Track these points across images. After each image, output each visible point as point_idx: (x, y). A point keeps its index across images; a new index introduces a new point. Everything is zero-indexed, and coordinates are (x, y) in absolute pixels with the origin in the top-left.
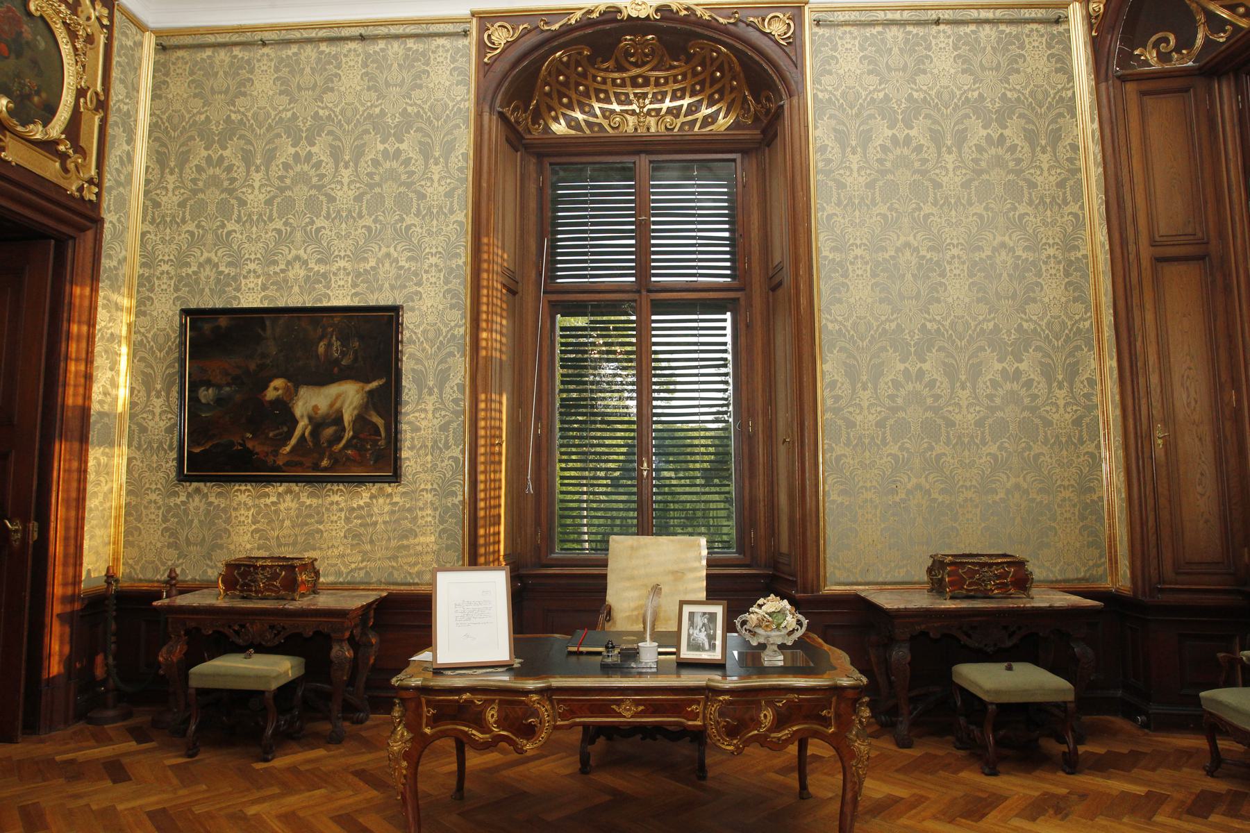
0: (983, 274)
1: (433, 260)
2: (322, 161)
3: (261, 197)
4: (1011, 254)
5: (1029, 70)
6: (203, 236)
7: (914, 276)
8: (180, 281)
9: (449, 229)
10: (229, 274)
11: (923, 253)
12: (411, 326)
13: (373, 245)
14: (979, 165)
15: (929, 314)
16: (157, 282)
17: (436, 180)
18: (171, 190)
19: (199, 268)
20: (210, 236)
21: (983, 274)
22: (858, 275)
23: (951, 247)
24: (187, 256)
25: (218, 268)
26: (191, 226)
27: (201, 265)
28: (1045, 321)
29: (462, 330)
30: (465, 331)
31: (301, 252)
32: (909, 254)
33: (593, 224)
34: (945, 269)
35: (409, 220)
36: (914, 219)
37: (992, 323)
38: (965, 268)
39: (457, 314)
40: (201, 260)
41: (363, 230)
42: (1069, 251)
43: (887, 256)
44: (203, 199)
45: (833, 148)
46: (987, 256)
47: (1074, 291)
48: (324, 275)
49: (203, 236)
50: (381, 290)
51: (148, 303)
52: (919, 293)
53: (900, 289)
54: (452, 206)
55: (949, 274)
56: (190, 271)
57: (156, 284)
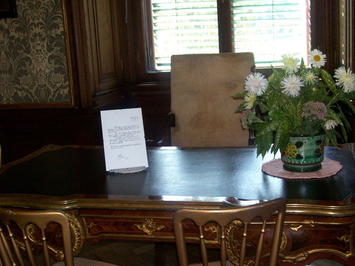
1: (37, 30)
7: (6, 53)
10: (19, 38)
15: (19, 85)
23: (33, 27)
25: (9, 33)
28: (34, 89)
29: (66, 91)
30: (70, 91)
39: (60, 77)
42: (50, 29)
47: (55, 64)
48: (24, 42)
55: (32, 50)
57: (32, 45)
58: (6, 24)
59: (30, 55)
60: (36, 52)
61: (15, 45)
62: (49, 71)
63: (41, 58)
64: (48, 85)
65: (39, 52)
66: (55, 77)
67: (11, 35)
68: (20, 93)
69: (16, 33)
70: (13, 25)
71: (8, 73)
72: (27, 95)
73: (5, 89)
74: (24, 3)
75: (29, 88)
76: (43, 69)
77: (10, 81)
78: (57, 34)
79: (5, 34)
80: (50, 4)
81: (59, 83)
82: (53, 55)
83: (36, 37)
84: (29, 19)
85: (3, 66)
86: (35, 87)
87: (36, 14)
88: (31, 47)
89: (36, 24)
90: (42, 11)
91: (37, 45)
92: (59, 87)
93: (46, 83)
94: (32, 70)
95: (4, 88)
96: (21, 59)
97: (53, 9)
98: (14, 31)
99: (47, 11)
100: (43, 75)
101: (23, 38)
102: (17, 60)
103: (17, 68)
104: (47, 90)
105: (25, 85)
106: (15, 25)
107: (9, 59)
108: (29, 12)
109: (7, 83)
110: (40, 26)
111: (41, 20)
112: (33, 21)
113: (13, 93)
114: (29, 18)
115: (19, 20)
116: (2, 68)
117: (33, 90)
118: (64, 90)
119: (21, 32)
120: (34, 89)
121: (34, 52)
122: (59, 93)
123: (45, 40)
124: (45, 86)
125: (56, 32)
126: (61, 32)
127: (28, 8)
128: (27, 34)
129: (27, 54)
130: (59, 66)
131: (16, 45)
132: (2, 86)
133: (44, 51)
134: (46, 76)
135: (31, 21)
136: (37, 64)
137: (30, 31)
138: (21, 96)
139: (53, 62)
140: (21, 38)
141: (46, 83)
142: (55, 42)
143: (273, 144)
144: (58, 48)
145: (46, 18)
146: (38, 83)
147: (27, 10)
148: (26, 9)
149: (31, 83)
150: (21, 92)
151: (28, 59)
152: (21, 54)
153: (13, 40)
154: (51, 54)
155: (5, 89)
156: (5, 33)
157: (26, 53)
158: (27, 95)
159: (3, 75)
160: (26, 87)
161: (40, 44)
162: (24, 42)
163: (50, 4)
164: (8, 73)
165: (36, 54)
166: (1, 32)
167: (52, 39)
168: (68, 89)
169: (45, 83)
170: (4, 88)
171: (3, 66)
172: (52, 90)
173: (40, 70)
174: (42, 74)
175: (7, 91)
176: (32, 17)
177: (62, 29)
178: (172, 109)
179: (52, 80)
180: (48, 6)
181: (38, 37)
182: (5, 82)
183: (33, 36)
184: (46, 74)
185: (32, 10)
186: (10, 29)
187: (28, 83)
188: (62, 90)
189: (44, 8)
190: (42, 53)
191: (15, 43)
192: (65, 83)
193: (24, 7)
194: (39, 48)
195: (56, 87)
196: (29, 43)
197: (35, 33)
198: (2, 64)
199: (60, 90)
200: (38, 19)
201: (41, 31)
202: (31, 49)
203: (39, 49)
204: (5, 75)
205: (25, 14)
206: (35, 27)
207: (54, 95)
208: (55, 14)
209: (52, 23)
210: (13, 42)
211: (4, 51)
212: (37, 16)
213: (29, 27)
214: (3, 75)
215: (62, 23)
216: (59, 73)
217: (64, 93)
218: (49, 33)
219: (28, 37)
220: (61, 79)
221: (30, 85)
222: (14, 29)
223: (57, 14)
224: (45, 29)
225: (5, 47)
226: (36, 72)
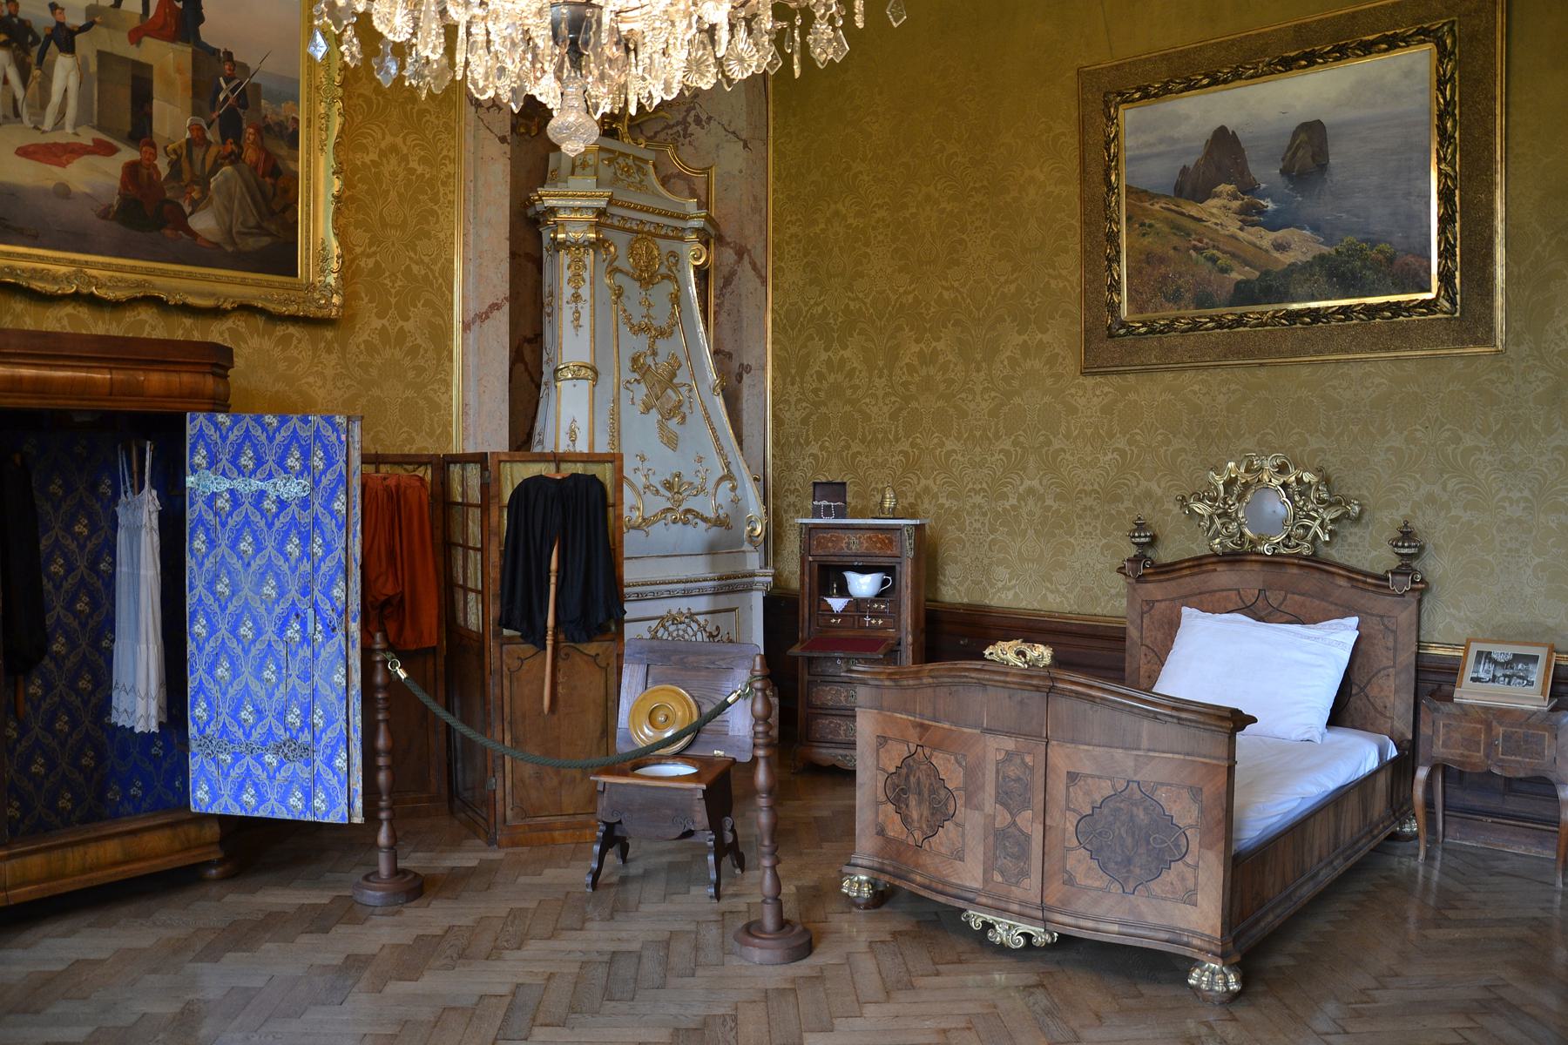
2: (855, 368)
4: (1039, 504)
5: (786, 286)
11: (1049, 502)
12: (954, 582)
14: (908, 390)
23: (1507, 504)
26: (1007, 444)
28: (965, 586)
38: (986, 522)
41: (1115, 455)
45: (956, 365)
50: (1024, 536)
53: (1020, 548)
56: (1122, 508)
57: (1077, 524)
64: (1096, 589)
72: (1062, 602)
84: (442, 149)
91: (1086, 524)
93: (1095, 586)
99: (995, 473)
106: (1464, 496)
108: (872, 472)
110: (1093, 496)
120: (965, 586)
125: (1117, 507)
135: (873, 485)
141: (1095, 586)
143: (881, 656)
154: (1542, 560)
172: (805, 309)
180: (1547, 467)
194: (978, 525)
201: (983, 501)
206: (1511, 505)
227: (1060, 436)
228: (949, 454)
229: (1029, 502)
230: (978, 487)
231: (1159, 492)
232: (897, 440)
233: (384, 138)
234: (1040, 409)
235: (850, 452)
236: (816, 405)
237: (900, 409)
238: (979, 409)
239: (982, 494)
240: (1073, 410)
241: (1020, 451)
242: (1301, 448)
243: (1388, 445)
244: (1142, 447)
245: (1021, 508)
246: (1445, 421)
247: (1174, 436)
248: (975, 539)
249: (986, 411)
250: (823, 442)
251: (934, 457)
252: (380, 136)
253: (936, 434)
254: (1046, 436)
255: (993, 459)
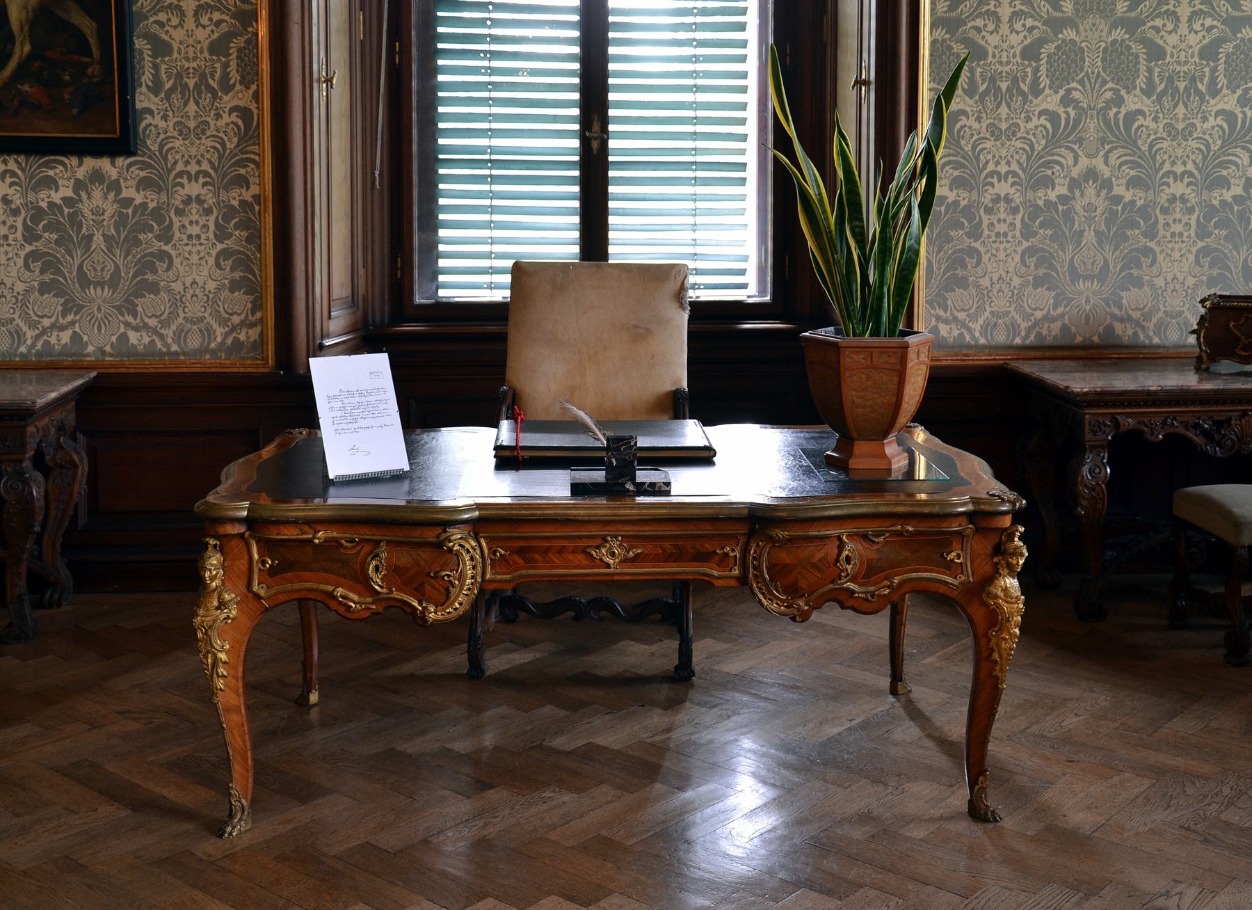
0: (54, 236)
1: (194, 189)
3: (1015, 39)
4: (111, 196)
6: (1077, 122)
8: (1033, 218)
9: (221, 123)
13: (1239, 151)
16: (986, 220)
17: (1005, 19)
18: (1184, 19)
19: (1070, 189)
20: (1092, 126)
21: (54, 236)
22: (998, 234)
23: (1171, 180)
24: (1048, 164)
25: (1111, 189)
26: (1051, 101)
27: (1074, 184)
31: (1098, 162)
32: (1093, 192)
33: (555, 119)
34: (1156, 221)
35: (1133, 102)
36: (1107, 122)
37: (69, 332)
38: (1193, 223)
40: (1075, 172)
41: (1219, 121)
42: (1034, 188)
43: (56, 197)
44: (1072, 41)
46: (1234, 197)
48: (1144, 212)
49: (1077, 122)
51: (1145, 261)
52: (116, 274)
53: (81, 266)
54: (1213, 79)
56: (1052, 196)
58: (113, 168)
59: (170, 245)
60: (1169, 239)
61: (1121, 216)
62: (1193, 283)
63: (7, 255)
65: (194, 241)
66: (38, 302)
67: (124, 194)
68: (133, 337)
69: (952, 191)
70: (133, 172)
71: (1096, 280)
73: (96, 325)
74: (166, 121)
75: (160, 325)
76: (200, 281)
77: (112, 307)
78: (244, 200)
79: (108, 193)
80: (233, 128)
81: (50, 317)
82: (1033, 246)
83: (189, 205)
84: (176, 163)
85: (95, 270)
86: (984, 318)
87: (1179, 152)
88: (1160, 226)
89: (193, 174)
90: (209, 145)
92: (48, 328)
93: (1185, 309)
94: (173, 282)
95: (93, 321)
96: (145, 254)
97: (1046, 144)
98: (1124, 186)
100: (200, 295)
101: (965, 202)
102: (946, 253)
103: (132, 276)
104: (1012, 325)
105: (149, 317)
107: (1102, 249)
108: (989, 145)
109: (103, 311)
110: (201, 180)
111: (205, 166)
112: (186, 166)
113: (116, 336)
114: (177, 158)
115: (1140, 160)
116: (93, 273)
117: (1152, 323)
118: (250, 331)
119: (1140, 189)
120: (173, 327)
121: (989, 237)
122: (47, 342)
123: (20, 213)
124: (11, 323)
126: (62, 199)
127: (988, 135)
128: (168, 196)
129: (162, 244)
130: (52, 277)
131: (134, 221)
132: (88, 318)
133: (1189, 237)
134: (208, 297)
136: (995, 265)
137: (987, 187)
138: (945, 335)
139: (1206, 261)
140: (149, 205)
142: (1217, 219)
144: (51, 236)
145: (219, 163)
146: (185, 313)
147: (172, 140)
148: (983, 138)
149: (974, 308)
150: (139, 334)
151: (1147, 251)
152: (146, 244)
153: (128, 208)
155: (96, 325)
156: (110, 189)
157: (969, 238)
158: (961, 334)
159: (1081, 284)
160: (961, 316)
161: (197, 222)
162: (968, 212)
163: (233, 128)
164: (1096, 280)
165: (187, 245)
166: (99, 186)
167: (1035, 211)
168: (258, 329)
169: (12, 316)
170: (93, 321)
171: (95, 270)
173: (192, 283)
174: (197, 291)
175: (99, 329)
176: (1170, 156)
177: (255, 190)
178: (507, 378)
179: (31, 308)
180: (1034, 134)
181: (194, 205)
182: (96, 307)
183: (183, 201)
184: (1012, 288)
185: (184, 139)
186: (122, 181)
187: (967, 307)
188: (55, 334)
189: (1024, 138)
190: (9, 245)
191: (134, 216)
192: (63, 318)
193: (979, 133)
194: (1178, 228)
195: (39, 326)
196: (171, 219)
197: (997, 194)
198: (94, 262)
199: (239, 331)
200: (1184, 163)
202: (173, 234)
203: (194, 234)
204: (99, 290)
205: (978, 149)
206: (190, 181)
207: (33, 345)
208: (1049, 155)
209: (42, 175)
210: (1117, 210)
211: (101, 232)
212: (195, 156)
213: (1161, 179)
214: (1081, 284)
215: (257, 174)
216: (239, 291)
217: (59, 341)
218: (1030, 196)
219: (979, 203)
220: (53, 308)
221: (163, 318)
222: (1125, 182)
223: (1229, 155)
224: (21, 187)
225: (105, 223)
226: (183, 287)
227: (1138, 91)
228: (1131, 116)
229: (1087, 192)
230: (1179, 169)
231: (1107, 173)
232: (1037, 91)
233: (1076, 163)
234: (1105, 50)
235: (1123, 111)
236: (1056, 25)
237: (1040, 42)
238: (1005, 46)
239: (1186, 180)
240: (1156, 53)
241: (1072, 113)
242: (1115, 110)
243: (1218, 108)
244: (1083, 108)
245: (1074, 198)
246: (1108, 79)
247: (1128, 93)
248: (997, 250)
249: (1196, 49)
250: (1069, 91)
251: (1107, 122)
252: (1071, 161)
253: (1110, 85)
254: (1116, 91)
255: (1206, 126)
